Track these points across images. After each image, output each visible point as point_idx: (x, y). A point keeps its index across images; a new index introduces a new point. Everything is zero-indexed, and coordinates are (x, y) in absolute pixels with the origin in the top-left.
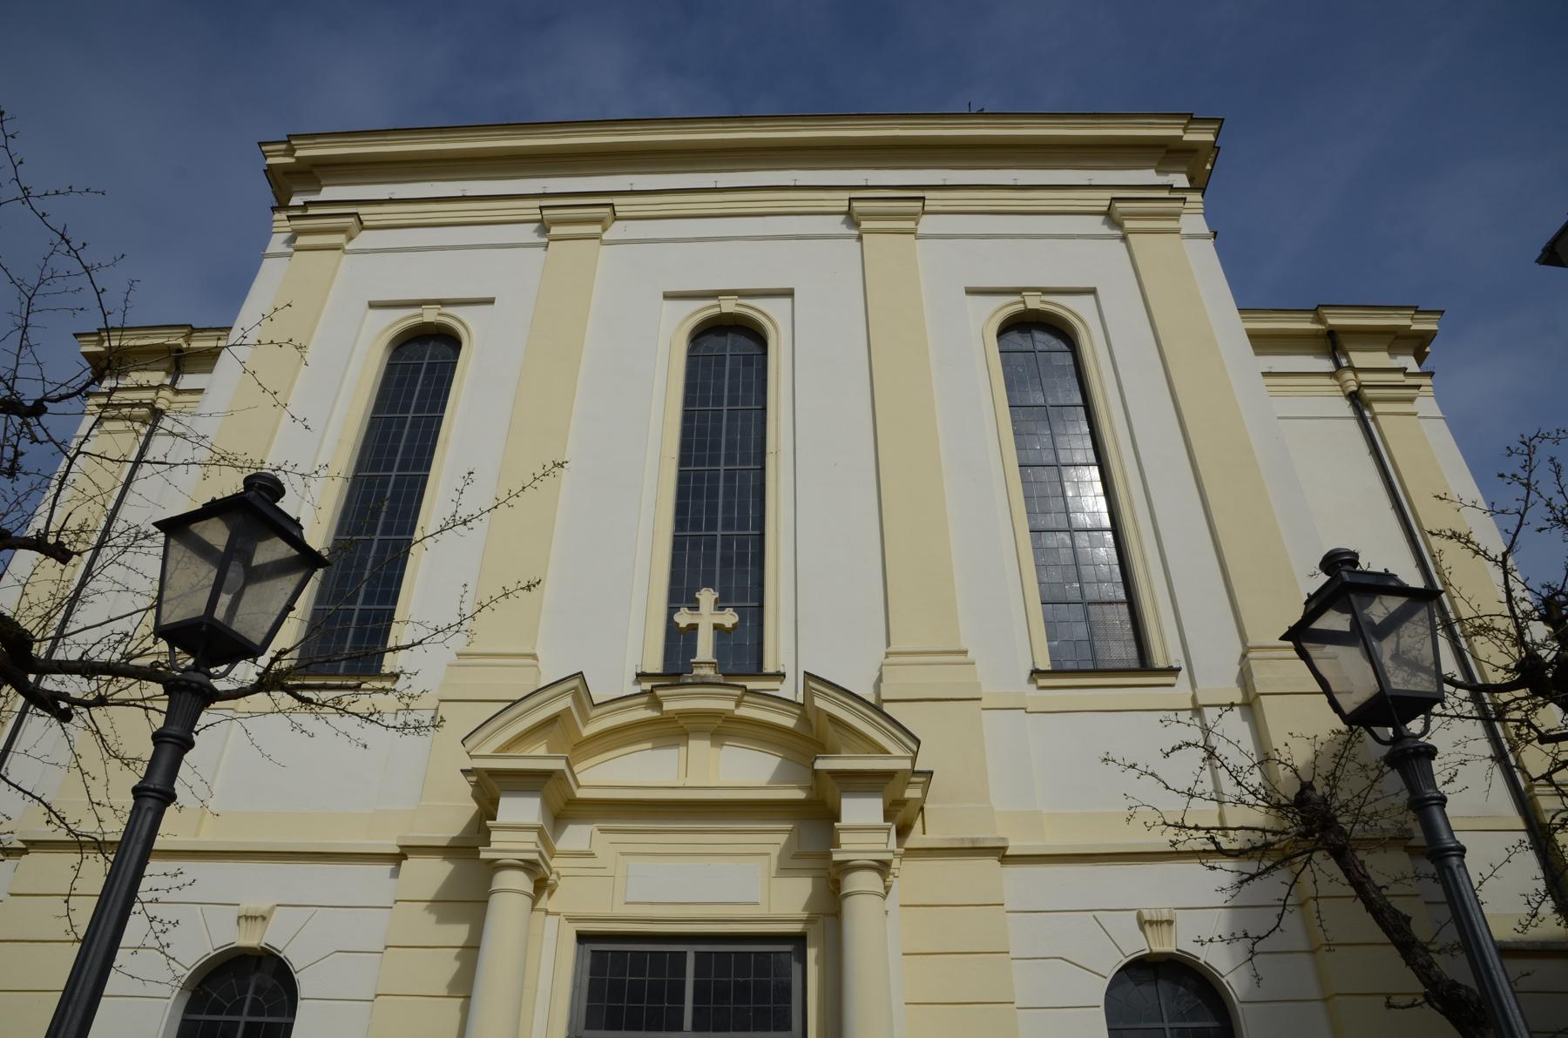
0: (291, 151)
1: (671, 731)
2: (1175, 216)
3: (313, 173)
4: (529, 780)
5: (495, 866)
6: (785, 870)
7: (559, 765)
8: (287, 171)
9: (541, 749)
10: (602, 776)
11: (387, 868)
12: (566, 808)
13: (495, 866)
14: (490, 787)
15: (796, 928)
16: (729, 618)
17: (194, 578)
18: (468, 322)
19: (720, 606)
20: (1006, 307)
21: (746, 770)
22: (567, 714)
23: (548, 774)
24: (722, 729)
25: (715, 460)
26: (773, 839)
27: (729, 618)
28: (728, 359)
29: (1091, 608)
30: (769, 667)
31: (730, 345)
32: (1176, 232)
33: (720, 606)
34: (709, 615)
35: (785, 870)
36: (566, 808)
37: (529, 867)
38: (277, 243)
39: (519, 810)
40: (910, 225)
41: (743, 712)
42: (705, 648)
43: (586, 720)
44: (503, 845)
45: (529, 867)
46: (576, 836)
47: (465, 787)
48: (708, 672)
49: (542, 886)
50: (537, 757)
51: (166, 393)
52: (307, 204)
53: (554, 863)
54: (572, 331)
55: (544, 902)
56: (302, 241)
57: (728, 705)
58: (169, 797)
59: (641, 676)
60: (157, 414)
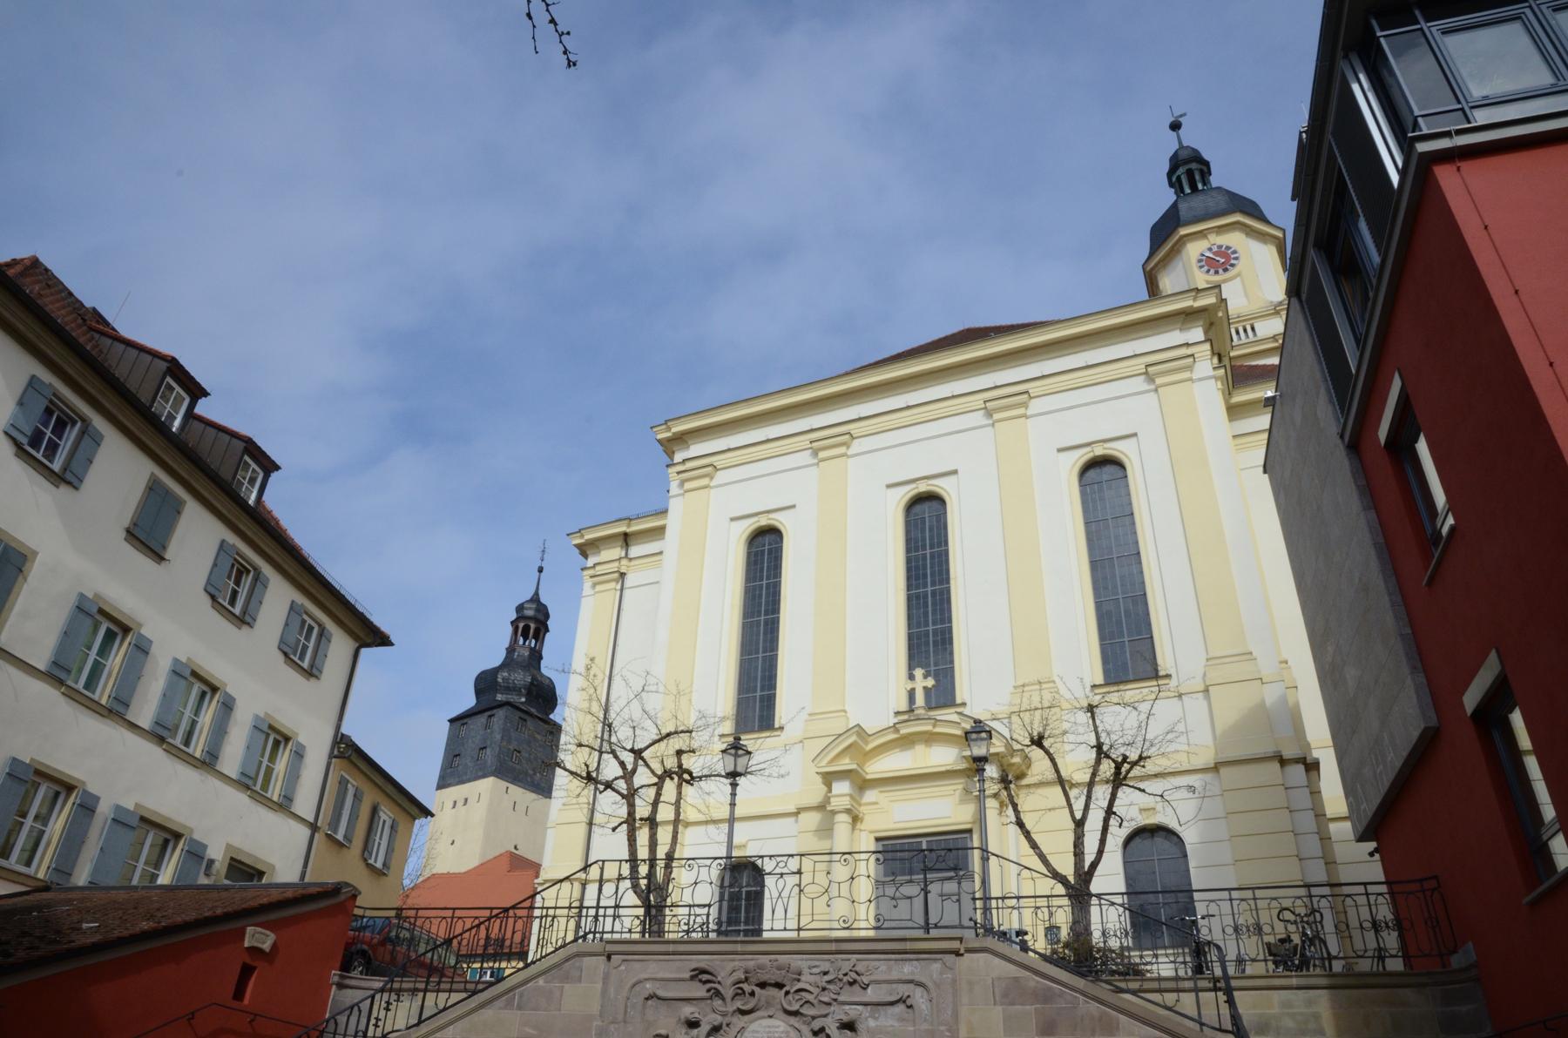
0: (669, 429)
1: (907, 742)
2: (1190, 368)
3: (682, 439)
4: (849, 770)
5: (834, 813)
6: (962, 801)
7: (854, 766)
8: (669, 440)
9: (847, 761)
10: (880, 767)
11: (792, 819)
12: (863, 784)
13: (834, 813)
14: (829, 778)
15: (968, 826)
16: (930, 682)
17: (730, 760)
18: (782, 521)
19: (925, 677)
20: (1083, 456)
21: (945, 756)
22: (859, 743)
23: (850, 771)
24: (930, 738)
25: (925, 586)
26: (958, 785)
27: (930, 682)
28: (926, 517)
29: (725, 826)
30: (959, 701)
31: (925, 509)
32: (1190, 379)
33: (925, 677)
34: (922, 682)
35: (962, 801)
36: (863, 784)
37: (848, 811)
38: (674, 488)
39: (842, 788)
40: (1021, 411)
41: (938, 730)
42: (920, 699)
43: (867, 743)
44: (836, 803)
45: (848, 811)
46: (871, 795)
47: (819, 779)
48: (921, 711)
49: (856, 819)
50: (846, 764)
51: (624, 562)
52: (684, 461)
53: (862, 809)
54: (839, 507)
55: (859, 826)
56: (688, 486)
57: (929, 728)
58: (1075, 855)
59: (897, 713)
60: (623, 575)
